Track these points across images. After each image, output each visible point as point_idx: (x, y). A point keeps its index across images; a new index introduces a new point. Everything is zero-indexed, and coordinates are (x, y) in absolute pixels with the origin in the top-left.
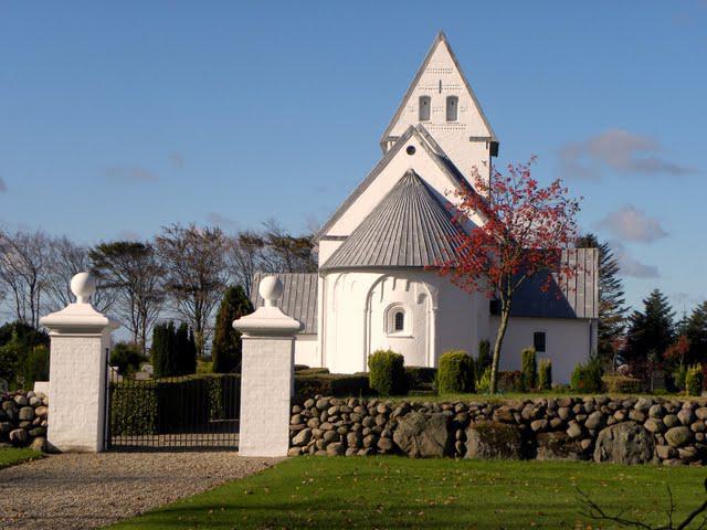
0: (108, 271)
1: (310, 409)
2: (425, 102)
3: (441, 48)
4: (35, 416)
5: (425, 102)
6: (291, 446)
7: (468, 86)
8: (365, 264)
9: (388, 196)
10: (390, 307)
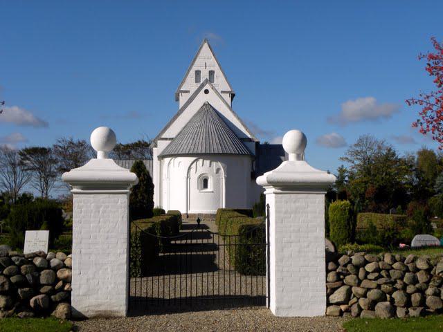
0: (28, 162)
1: (345, 266)
2: (198, 73)
3: (206, 45)
4: (57, 280)
5: (198, 73)
6: (329, 304)
7: (219, 65)
8: (187, 152)
9: (195, 116)
10: (200, 176)
